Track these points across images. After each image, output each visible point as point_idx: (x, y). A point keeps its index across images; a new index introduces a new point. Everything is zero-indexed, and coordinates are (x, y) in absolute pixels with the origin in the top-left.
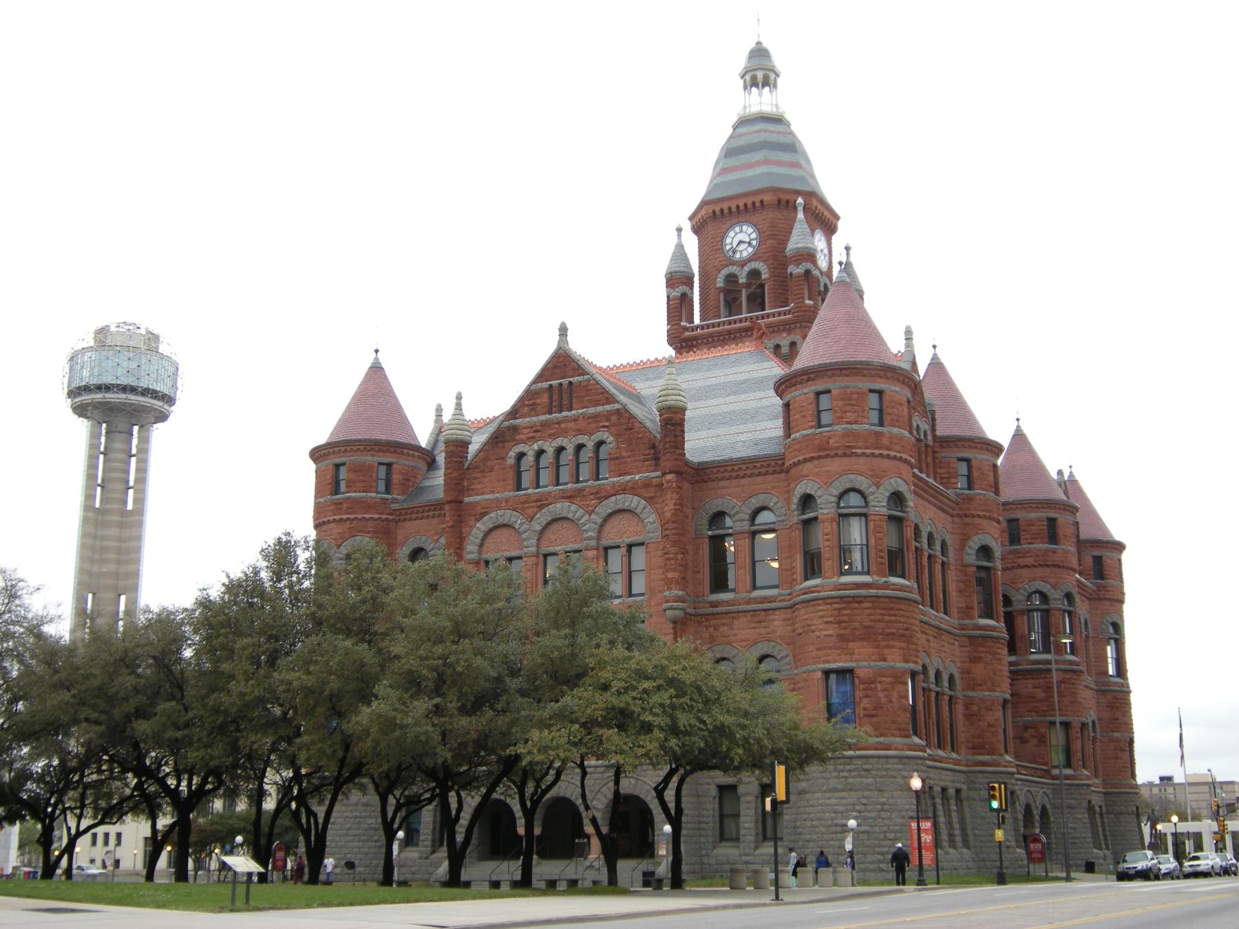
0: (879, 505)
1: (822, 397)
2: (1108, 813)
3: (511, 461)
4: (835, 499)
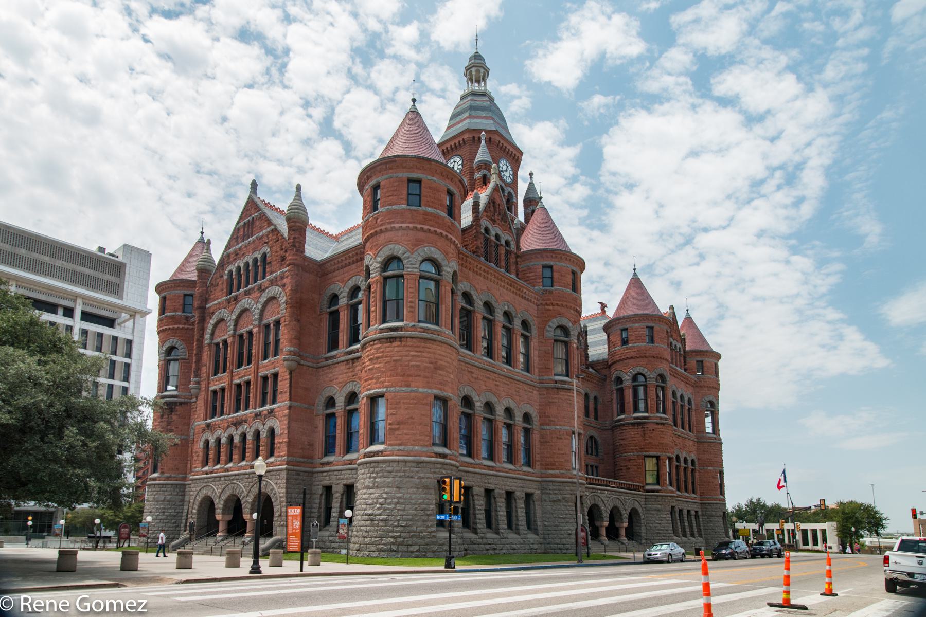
2: (703, 515)
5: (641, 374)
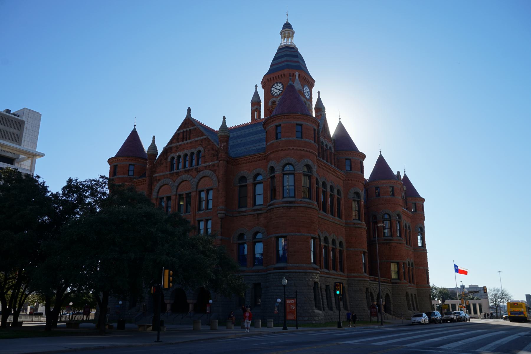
0: (301, 169)
1: (278, 128)
3: (169, 160)
4: (281, 168)
5: (387, 214)
